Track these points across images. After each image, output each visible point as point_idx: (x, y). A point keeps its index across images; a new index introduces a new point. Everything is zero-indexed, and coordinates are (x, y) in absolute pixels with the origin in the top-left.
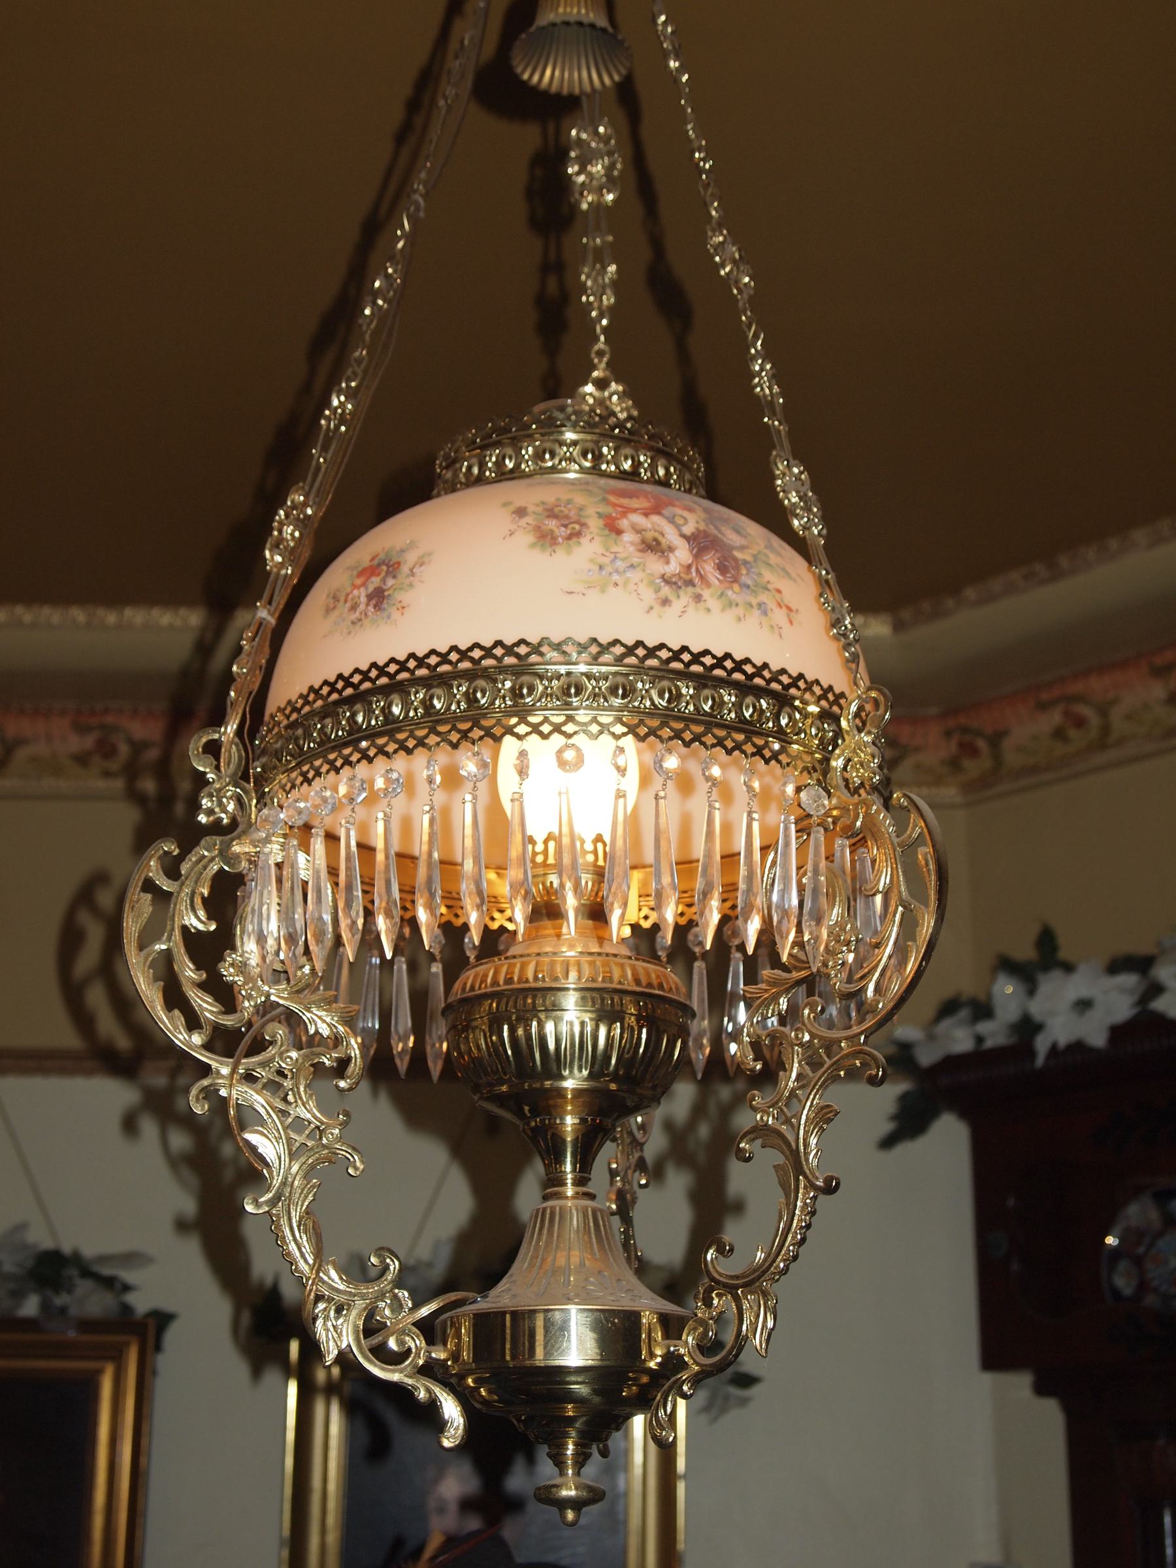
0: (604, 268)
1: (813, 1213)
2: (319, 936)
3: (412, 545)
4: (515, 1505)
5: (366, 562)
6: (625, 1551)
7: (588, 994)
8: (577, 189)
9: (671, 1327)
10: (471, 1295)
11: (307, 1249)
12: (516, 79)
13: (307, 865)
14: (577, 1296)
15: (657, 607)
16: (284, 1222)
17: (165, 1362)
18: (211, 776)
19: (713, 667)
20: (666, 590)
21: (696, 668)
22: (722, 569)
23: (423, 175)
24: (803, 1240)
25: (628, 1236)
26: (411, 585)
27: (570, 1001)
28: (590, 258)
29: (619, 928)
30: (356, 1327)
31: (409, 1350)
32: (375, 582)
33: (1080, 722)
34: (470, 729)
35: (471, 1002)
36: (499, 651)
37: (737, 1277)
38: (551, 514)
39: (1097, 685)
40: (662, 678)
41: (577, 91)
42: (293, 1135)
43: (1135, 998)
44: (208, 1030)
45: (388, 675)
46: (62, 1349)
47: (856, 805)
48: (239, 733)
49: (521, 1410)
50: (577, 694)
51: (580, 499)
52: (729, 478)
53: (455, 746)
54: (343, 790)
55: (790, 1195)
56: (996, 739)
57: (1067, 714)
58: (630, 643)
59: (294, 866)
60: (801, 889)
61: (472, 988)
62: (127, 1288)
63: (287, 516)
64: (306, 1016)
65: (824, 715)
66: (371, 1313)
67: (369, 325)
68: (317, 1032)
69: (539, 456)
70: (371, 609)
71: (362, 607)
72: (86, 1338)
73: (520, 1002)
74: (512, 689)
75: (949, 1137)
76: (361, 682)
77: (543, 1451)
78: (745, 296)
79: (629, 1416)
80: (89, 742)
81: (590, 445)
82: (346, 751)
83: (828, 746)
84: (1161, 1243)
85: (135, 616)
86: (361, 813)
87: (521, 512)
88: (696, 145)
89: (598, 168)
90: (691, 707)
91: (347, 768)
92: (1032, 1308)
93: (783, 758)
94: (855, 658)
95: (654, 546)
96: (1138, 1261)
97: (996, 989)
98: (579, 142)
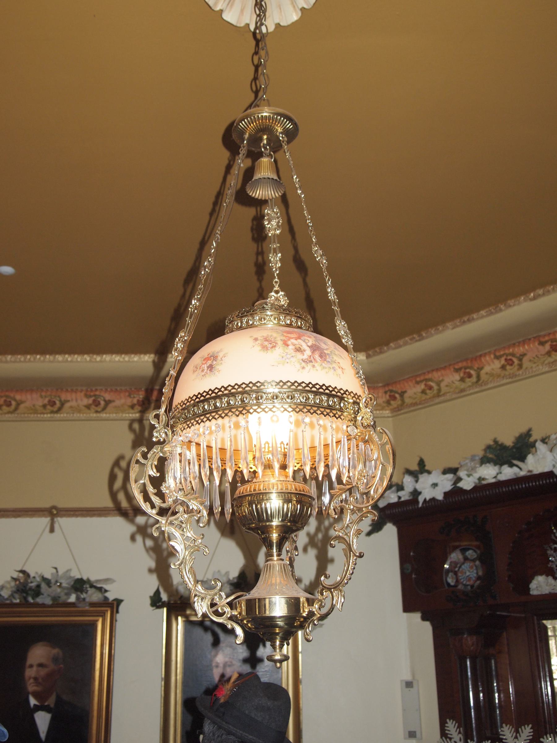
0: (277, 255)
1: (355, 564)
2: (195, 478)
3: (221, 351)
4: (261, 660)
5: (206, 356)
6: (281, 679)
7: (280, 494)
8: (268, 229)
9: (310, 602)
10: (245, 593)
11: (192, 580)
12: (248, 195)
13: (189, 455)
14: (280, 593)
15: (301, 370)
16: (184, 571)
17: (119, 616)
18: (157, 425)
19: (319, 389)
20: (303, 364)
21: (314, 389)
22: (321, 356)
23: (219, 228)
24: (353, 573)
25: (293, 572)
26: (221, 364)
27: (274, 496)
28: (272, 251)
29: (290, 471)
30: (207, 604)
31: (225, 612)
32: (209, 362)
33: (431, 388)
34: (242, 410)
35: (242, 497)
36: (251, 385)
37: (331, 585)
38: (266, 340)
39: (436, 375)
40: (303, 393)
41: (267, 198)
42: (186, 542)
43: (452, 482)
44: (157, 508)
45: (215, 393)
46: (83, 613)
47: (366, 432)
48: (166, 411)
49: (260, 630)
50: (276, 398)
51: (275, 335)
52: (322, 327)
53: (238, 416)
54: (201, 430)
55: (348, 558)
56: (402, 394)
57: (426, 385)
58: (293, 382)
59: (185, 455)
60: (349, 459)
61: (243, 493)
62: (106, 591)
63: (179, 340)
64: (189, 504)
65: (354, 403)
66: (213, 599)
67: (203, 277)
68: (193, 508)
69: (260, 319)
70: (208, 371)
71: (206, 371)
72: (92, 609)
73: (258, 497)
74: (256, 397)
75: (390, 531)
76: (206, 395)
77: (268, 644)
78: (325, 267)
79: (296, 632)
80: (90, 401)
81: (276, 316)
82: (202, 418)
83: (356, 413)
84: (463, 567)
85: (107, 357)
86: (207, 437)
87: (256, 339)
88: (307, 218)
89: (274, 223)
90: (313, 402)
91: (202, 423)
92: (421, 590)
93: (342, 417)
94: (364, 384)
95: (299, 350)
96: (456, 573)
97: (405, 480)
98: (268, 214)
